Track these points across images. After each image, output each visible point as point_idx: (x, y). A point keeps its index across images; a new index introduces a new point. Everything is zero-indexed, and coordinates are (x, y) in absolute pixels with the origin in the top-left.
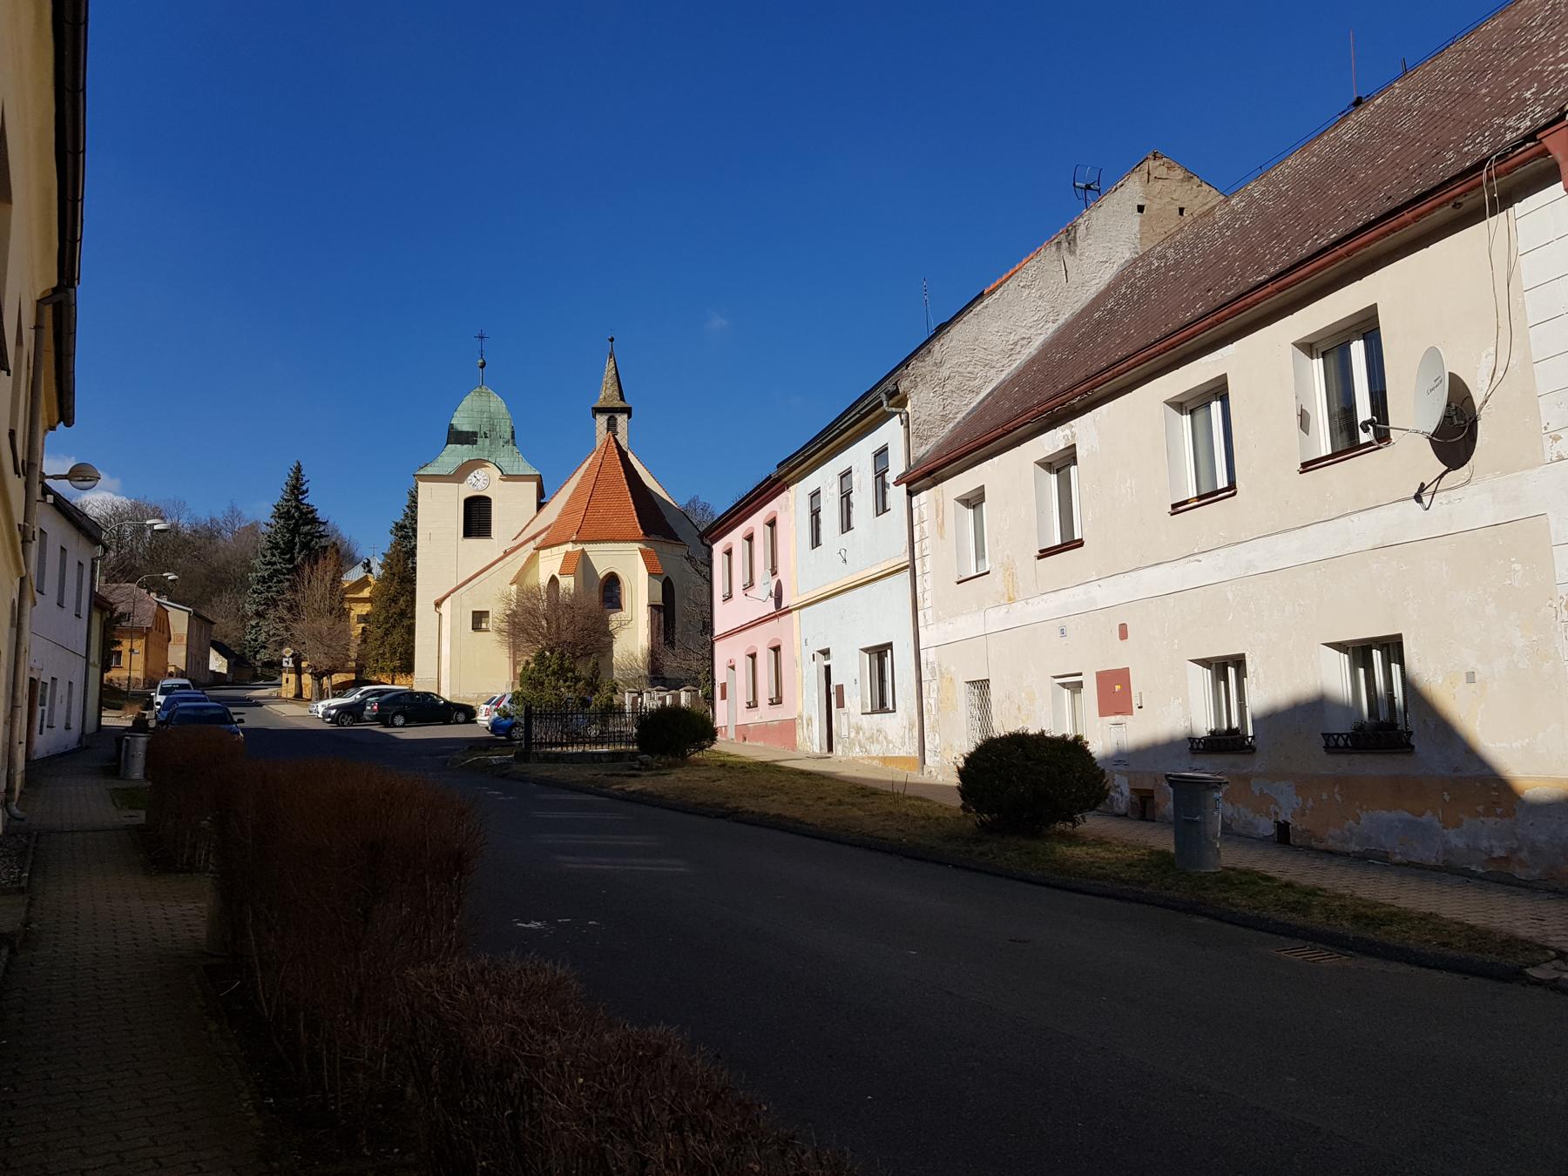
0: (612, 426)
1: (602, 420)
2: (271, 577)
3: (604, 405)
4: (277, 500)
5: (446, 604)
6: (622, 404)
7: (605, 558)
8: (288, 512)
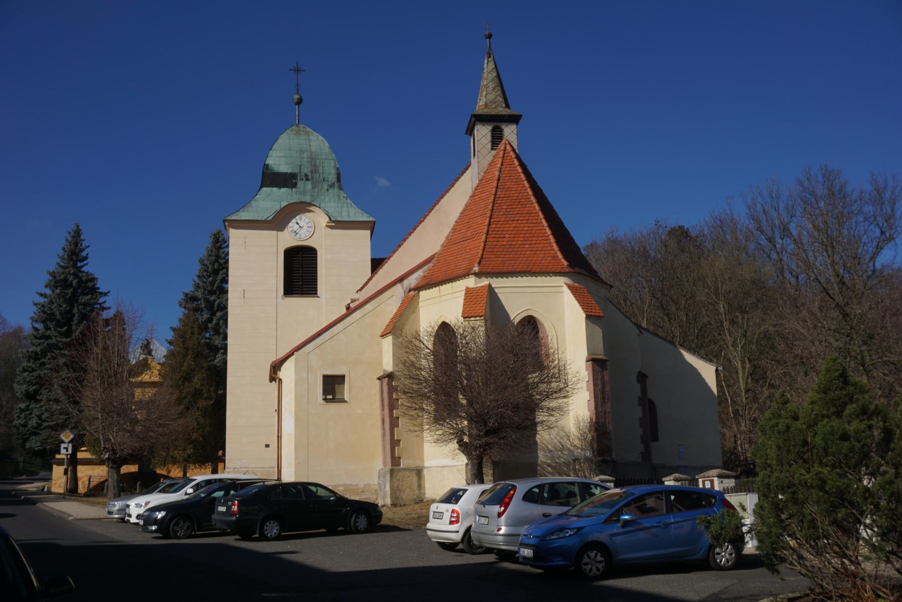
0: (497, 137)
1: (483, 133)
2: (44, 353)
3: (486, 111)
4: (53, 267)
5: (287, 372)
6: (506, 112)
7: (519, 296)
8: (65, 280)
